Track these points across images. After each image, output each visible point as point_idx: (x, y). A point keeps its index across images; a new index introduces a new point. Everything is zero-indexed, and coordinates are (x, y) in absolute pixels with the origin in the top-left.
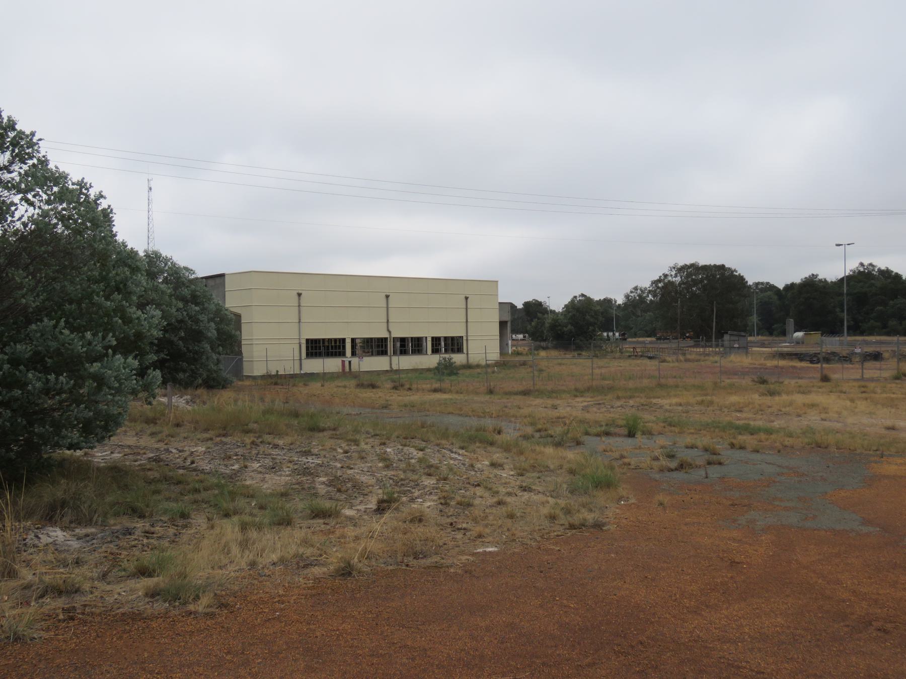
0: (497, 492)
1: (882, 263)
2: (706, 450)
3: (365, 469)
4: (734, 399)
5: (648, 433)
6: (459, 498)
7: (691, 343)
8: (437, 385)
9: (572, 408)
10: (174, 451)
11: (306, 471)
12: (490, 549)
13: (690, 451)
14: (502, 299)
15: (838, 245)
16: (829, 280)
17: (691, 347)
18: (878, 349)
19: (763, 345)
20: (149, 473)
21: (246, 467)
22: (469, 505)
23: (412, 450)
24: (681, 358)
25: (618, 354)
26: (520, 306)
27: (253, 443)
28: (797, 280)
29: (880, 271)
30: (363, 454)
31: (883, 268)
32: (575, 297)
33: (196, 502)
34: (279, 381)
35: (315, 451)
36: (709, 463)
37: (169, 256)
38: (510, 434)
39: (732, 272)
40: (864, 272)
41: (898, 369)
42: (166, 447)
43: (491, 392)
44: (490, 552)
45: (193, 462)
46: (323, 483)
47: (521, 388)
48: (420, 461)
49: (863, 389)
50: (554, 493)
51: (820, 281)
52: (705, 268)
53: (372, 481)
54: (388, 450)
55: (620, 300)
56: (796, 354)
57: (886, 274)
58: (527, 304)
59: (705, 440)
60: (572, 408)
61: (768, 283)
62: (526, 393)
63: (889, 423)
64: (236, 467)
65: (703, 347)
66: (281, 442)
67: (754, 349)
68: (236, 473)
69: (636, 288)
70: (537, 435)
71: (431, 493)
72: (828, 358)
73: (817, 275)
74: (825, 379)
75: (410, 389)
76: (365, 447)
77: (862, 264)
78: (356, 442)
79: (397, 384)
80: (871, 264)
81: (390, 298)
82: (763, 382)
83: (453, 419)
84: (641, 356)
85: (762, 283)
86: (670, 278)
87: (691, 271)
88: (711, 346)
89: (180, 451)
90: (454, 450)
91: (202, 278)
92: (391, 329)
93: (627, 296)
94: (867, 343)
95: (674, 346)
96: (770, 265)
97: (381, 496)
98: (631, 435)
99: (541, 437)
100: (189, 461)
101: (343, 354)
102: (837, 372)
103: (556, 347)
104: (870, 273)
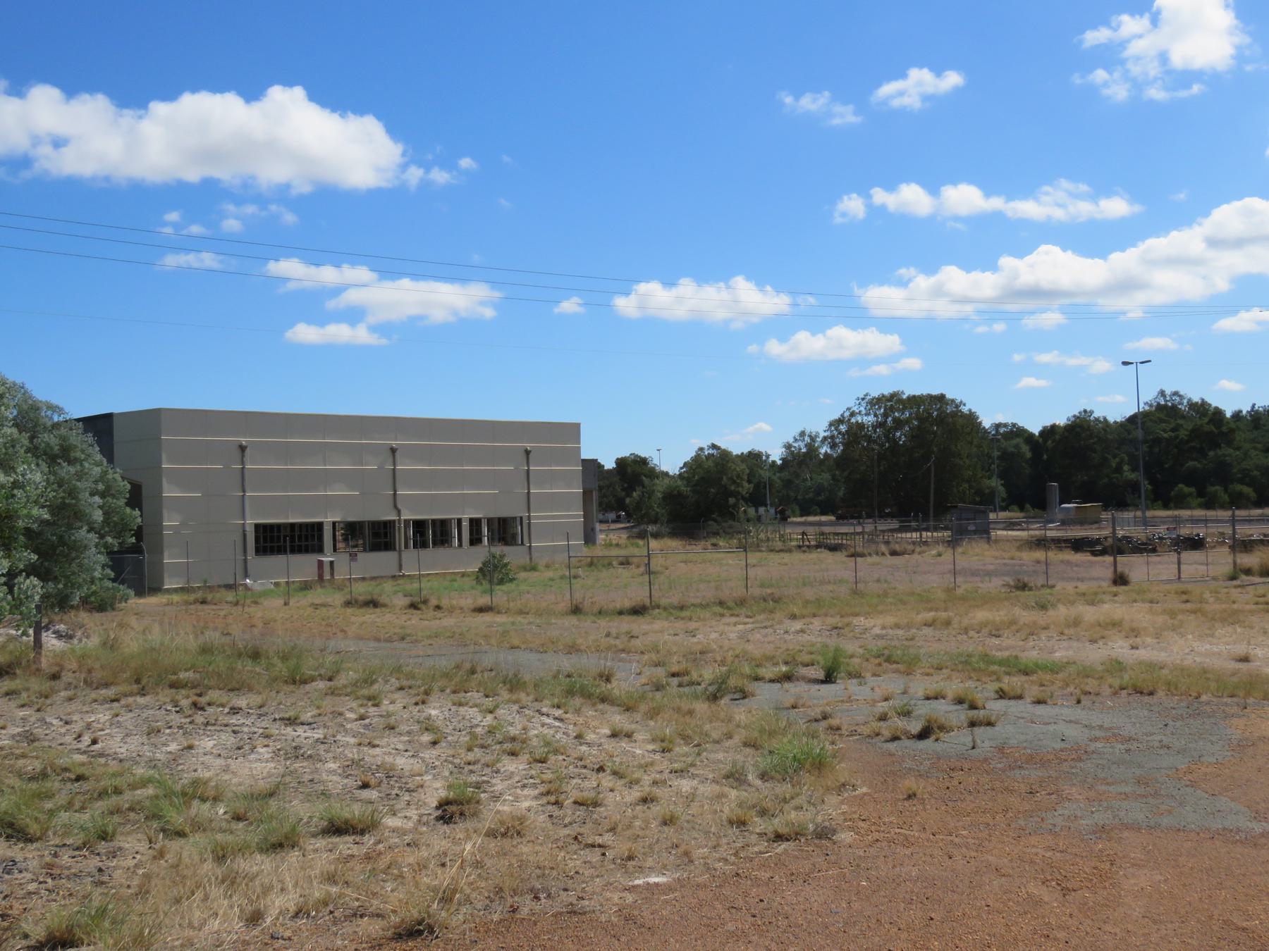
0: (637, 782)
1: (1194, 392)
2: (960, 701)
3: (400, 747)
4: (981, 615)
5: (856, 675)
6: (574, 795)
7: (895, 524)
8: (484, 600)
9: (725, 635)
10: (55, 722)
11: (296, 752)
12: (656, 880)
13: (934, 703)
14: (585, 455)
15: (1125, 363)
16: (1111, 420)
17: (892, 531)
18: (142, 601)
19: (1010, 525)
20: (21, 762)
21: (190, 747)
22: (596, 804)
23: (472, 712)
24: (883, 548)
25: (779, 545)
26: (609, 464)
27: (195, 704)
28: (1061, 420)
29: (1192, 405)
30: (392, 720)
31: (1196, 399)
32: (701, 449)
33: (117, 811)
34: (209, 597)
35: (307, 716)
36: (972, 724)
37: (19, 381)
38: (626, 682)
39: (957, 406)
40: (1166, 406)
41: (1235, 563)
42: (39, 715)
43: (576, 610)
44: (657, 885)
45: (94, 742)
46: (333, 772)
47: (627, 604)
48: (491, 731)
49: (1185, 597)
50: (735, 777)
51: (1097, 420)
52: (915, 401)
53: (416, 765)
54: (433, 712)
55: (776, 454)
56: (1067, 541)
57: (1201, 409)
58: (621, 463)
59: (954, 687)
60: (725, 635)
61: (1014, 425)
62: (638, 611)
63: (1241, 649)
64: (173, 747)
65: (916, 530)
66: (242, 702)
67: (999, 532)
68: (175, 759)
69: (803, 434)
70: (675, 681)
71: (524, 786)
72: (1120, 547)
73: (1092, 412)
74: (1120, 580)
75: (438, 607)
76: (391, 708)
77: (1162, 393)
78: (374, 700)
79: (416, 599)
80: (1176, 393)
81: (531, 455)
82: (1023, 587)
83: (525, 658)
84: (817, 547)
85: (1005, 425)
86: (859, 419)
87: (891, 403)
88: (927, 530)
89: (67, 723)
90: (544, 710)
91: (78, 420)
92: (399, 506)
93: (788, 446)
94: (1178, 521)
95: (869, 527)
96: (1021, 396)
97: (443, 794)
98: (829, 679)
99: (680, 685)
100: (87, 739)
101: (320, 550)
102: (1135, 566)
103: (674, 534)
104: (1174, 407)
